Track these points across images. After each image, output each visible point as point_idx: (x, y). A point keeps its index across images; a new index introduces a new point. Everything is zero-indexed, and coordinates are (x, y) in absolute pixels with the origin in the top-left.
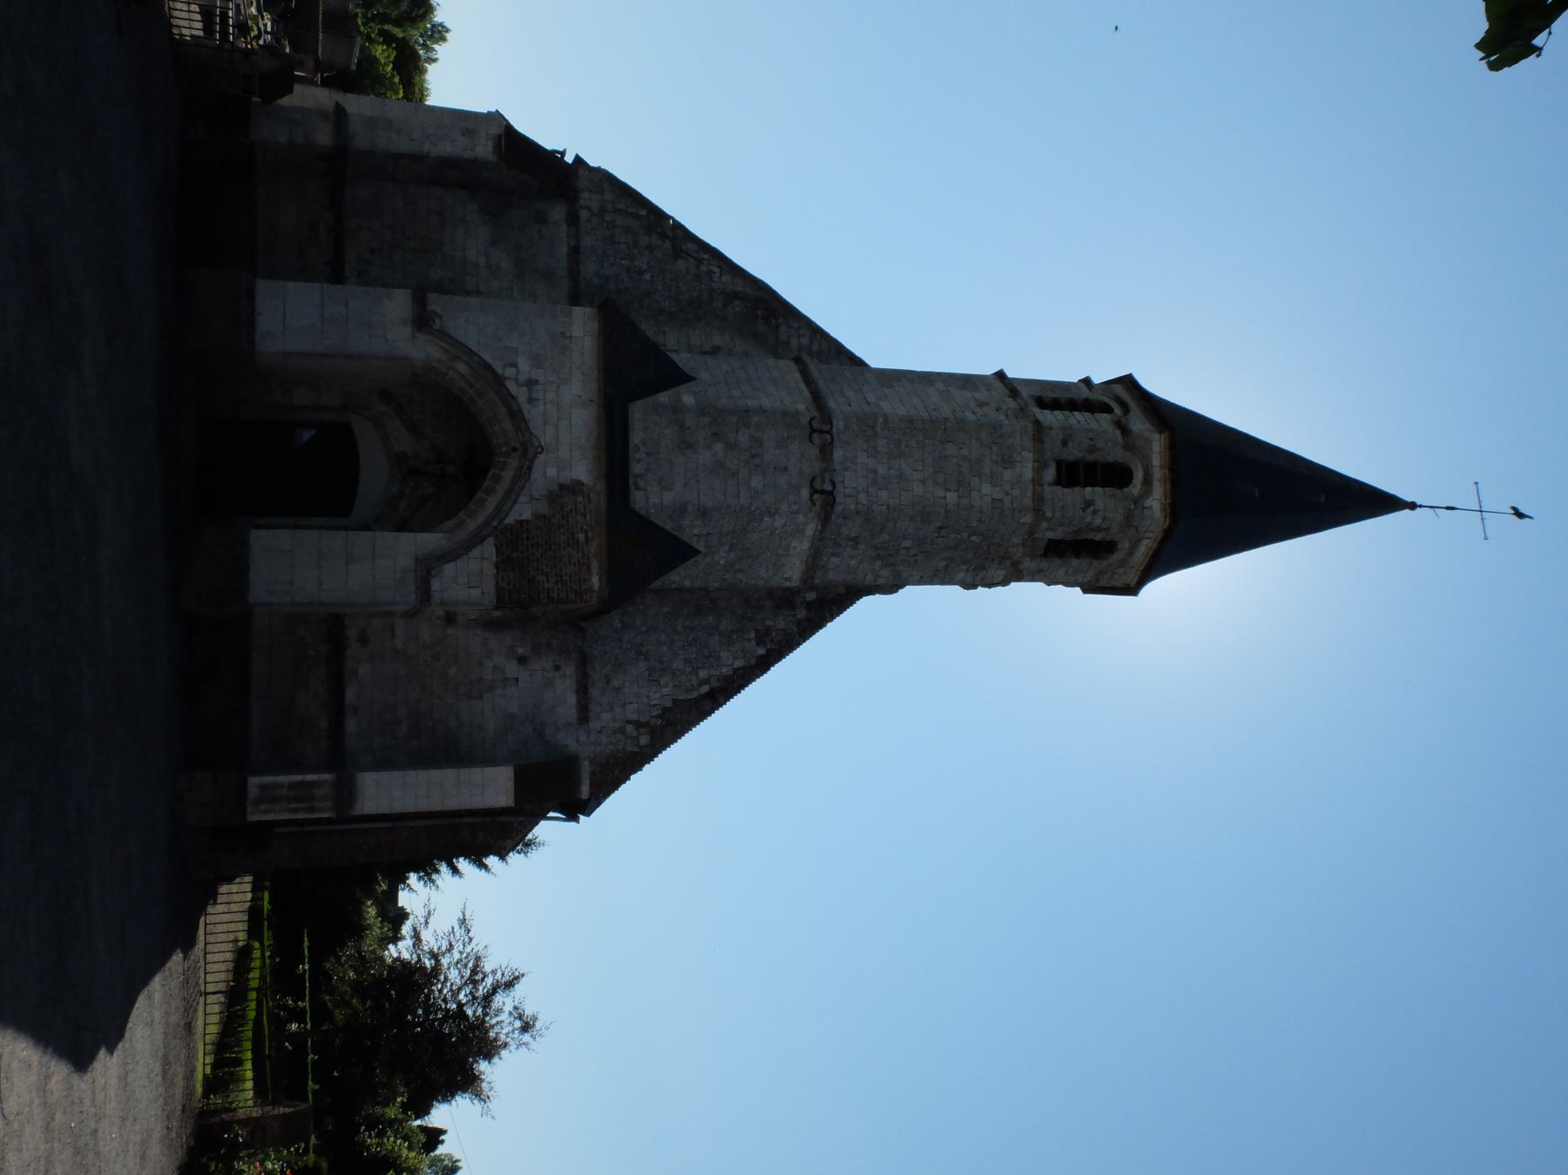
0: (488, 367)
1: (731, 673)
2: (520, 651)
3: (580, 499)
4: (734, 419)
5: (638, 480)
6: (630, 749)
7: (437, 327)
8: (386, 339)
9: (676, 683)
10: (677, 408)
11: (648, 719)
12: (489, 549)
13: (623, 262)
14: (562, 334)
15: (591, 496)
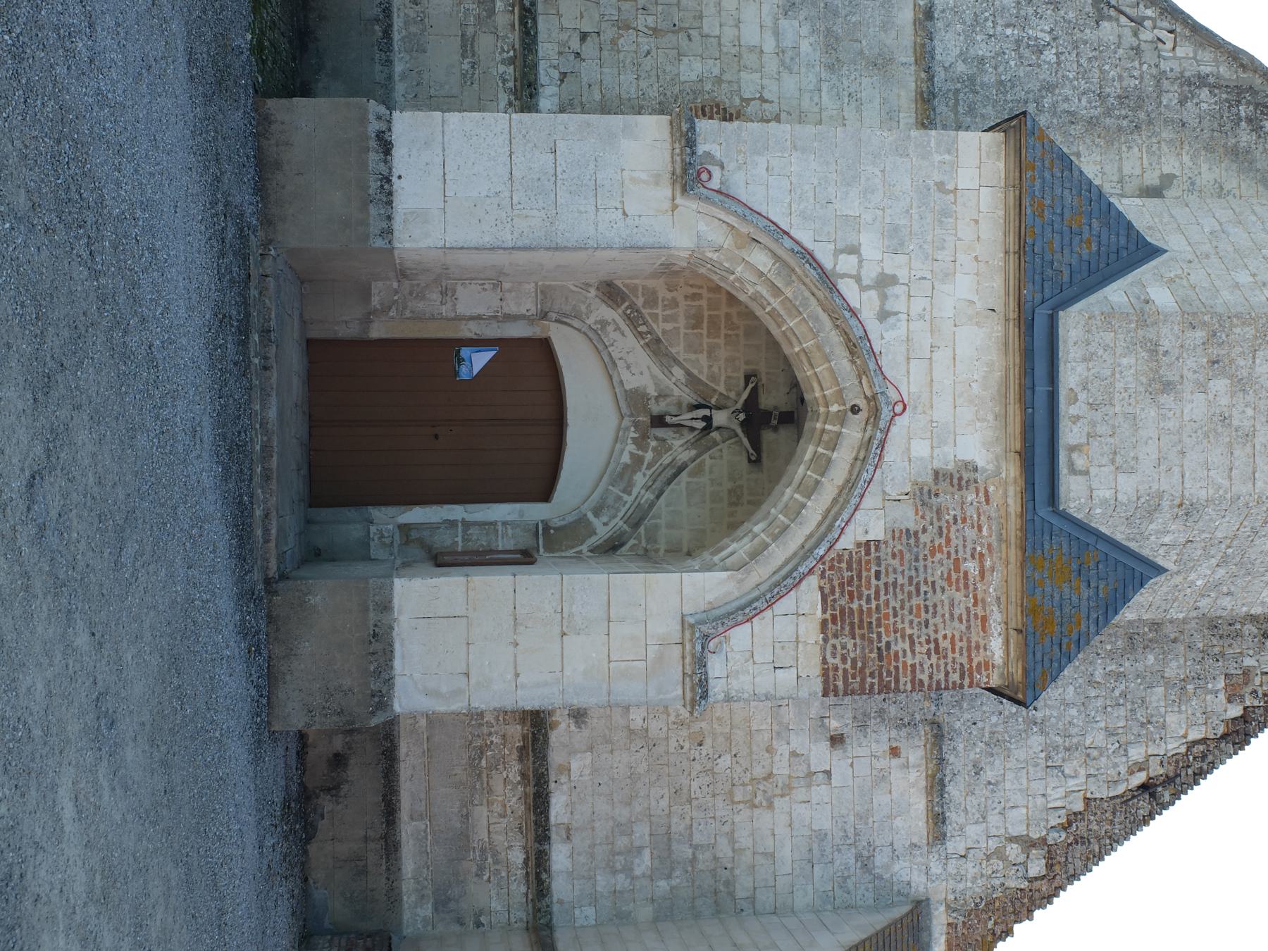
0: (808, 256)
1: (1183, 750)
2: (834, 724)
3: (971, 497)
4: (1250, 332)
5: (1075, 455)
6: (1012, 884)
7: (715, 183)
8: (624, 214)
9: (1092, 771)
10: (1144, 315)
11: (1044, 833)
12: (809, 596)
13: (1009, 31)
14: (940, 186)
15: (991, 489)
